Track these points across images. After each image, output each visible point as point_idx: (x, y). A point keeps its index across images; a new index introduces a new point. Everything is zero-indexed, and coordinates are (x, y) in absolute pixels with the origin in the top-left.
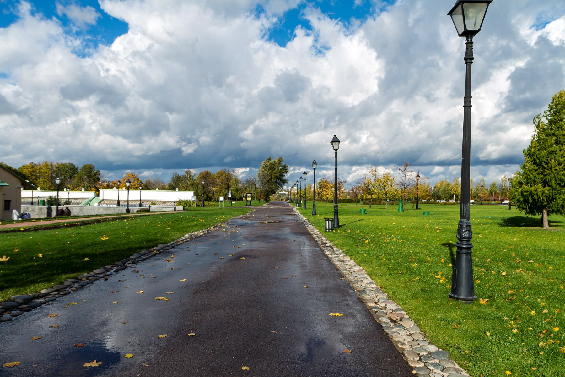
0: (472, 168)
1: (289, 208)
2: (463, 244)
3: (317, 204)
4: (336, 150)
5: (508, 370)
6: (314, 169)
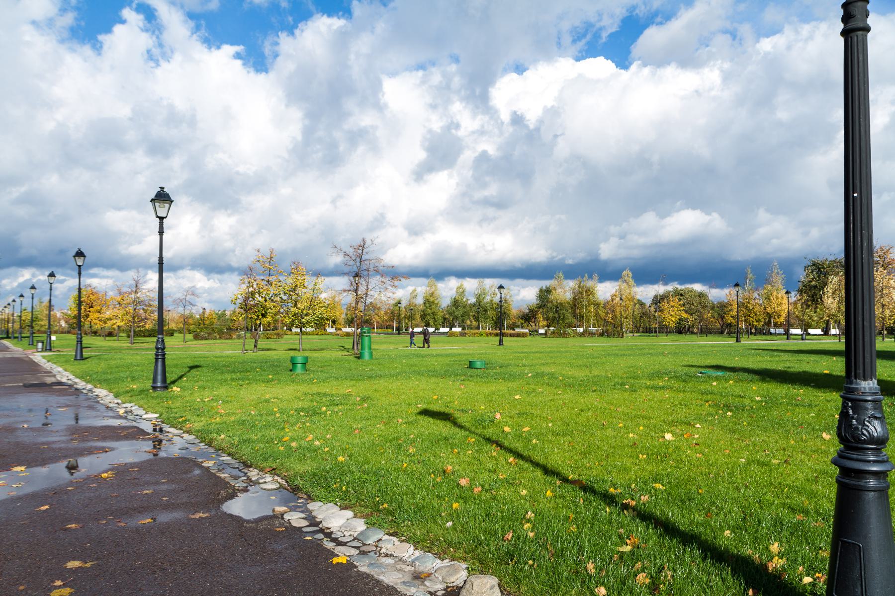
0: (841, 256)
1: (8, 355)
2: (869, 461)
3: (86, 340)
4: (161, 219)
5: (605, 587)
6: (80, 266)
